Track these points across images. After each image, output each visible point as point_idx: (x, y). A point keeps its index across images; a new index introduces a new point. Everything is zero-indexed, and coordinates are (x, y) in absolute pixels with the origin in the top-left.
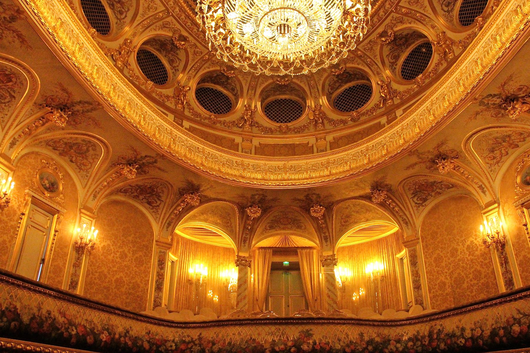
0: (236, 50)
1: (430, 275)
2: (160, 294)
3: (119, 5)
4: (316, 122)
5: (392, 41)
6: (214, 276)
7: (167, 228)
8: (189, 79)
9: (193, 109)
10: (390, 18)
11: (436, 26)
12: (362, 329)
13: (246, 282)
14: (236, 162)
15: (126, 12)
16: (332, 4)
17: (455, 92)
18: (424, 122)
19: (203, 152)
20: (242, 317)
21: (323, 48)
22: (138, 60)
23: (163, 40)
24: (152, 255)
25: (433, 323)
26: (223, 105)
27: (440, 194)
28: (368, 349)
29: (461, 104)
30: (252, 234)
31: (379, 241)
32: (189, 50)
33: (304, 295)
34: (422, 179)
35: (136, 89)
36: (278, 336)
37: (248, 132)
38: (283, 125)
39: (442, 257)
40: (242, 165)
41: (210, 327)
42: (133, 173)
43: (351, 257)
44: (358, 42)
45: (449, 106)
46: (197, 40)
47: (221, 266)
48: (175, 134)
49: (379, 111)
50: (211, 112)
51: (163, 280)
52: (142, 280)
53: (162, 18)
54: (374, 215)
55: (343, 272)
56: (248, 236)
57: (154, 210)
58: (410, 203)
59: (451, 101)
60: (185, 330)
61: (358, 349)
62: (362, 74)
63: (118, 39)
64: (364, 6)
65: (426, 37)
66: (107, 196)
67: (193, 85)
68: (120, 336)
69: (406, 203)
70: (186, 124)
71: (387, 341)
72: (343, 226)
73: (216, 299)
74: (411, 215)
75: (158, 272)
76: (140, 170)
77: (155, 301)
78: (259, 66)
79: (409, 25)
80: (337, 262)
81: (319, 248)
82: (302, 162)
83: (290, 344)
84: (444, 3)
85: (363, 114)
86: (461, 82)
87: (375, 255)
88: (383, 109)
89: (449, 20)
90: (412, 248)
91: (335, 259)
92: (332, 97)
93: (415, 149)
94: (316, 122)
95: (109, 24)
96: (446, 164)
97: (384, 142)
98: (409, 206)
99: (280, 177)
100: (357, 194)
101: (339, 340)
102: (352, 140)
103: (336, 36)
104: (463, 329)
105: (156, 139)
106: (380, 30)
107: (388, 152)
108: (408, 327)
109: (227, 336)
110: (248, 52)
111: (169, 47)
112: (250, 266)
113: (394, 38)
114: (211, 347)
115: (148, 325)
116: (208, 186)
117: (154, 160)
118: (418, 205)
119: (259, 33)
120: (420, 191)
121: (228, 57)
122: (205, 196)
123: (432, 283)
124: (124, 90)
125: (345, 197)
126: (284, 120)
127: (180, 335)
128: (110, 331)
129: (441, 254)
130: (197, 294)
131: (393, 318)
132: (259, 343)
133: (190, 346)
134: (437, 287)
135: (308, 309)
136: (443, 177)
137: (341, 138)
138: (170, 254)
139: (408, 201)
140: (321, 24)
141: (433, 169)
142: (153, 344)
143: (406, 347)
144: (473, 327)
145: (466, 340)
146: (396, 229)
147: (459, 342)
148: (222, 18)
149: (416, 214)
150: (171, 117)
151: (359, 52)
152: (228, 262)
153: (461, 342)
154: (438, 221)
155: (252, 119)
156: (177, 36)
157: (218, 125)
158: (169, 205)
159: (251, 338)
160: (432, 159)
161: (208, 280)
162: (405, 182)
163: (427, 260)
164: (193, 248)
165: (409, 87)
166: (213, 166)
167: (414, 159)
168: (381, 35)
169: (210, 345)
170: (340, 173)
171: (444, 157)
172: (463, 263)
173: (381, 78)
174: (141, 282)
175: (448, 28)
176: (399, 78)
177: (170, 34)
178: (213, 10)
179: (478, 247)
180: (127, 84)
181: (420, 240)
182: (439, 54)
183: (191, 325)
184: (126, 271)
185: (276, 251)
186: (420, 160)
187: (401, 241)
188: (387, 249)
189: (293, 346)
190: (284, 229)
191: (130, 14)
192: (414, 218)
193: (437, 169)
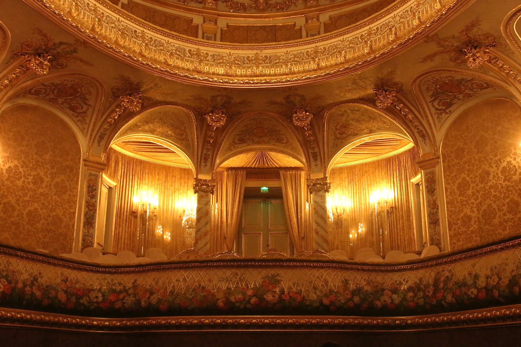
2: (91, 231)
7: (99, 142)
12: (347, 275)
13: (207, 213)
19: (143, 37)
24: (78, 178)
25: (440, 268)
28: (353, 301)
30: (216, 149)
31: (389, 160)
33: (288, 230)
34: (447, 74)
40: (198, 54)
41: (148, 271)
43: (351, 181)
47: (177, 192)
48: (101, 11)
51: (96, 212)
52: (65, 212)
54: (381, 124)
55: (339, 201)
56: (210, 153)
57: (80, 118)
61: (339, 301)
66: (10, 99)
68: (25, 285)
69: (423, 109)
71: (379, 291)
72: (338, 139)
73: (168, 237)
74: (430, 125)
75: (87, 202)
76: (54, 63)
77: (84, 240)
80: (330, 187)
82: (280, 51)
83: (250, 293)
87: (382, 179)
91: (327, 183)
93: (433, 33)
96: (478, 55)
99: (249, 72)
100: (356, 96)
101: (315, 288)
105: (73, 18)
107: (397, 38)
109: (169, 283)
114: (149, 298)
115: (65, 270)
116: (152, 85)
118: (440, 112)
120: (443, 93)
122: (149, 99)
123: (453, 217)
125: (338, 99)
127: (108, 282)
128: (9, 278)
129: (468, 179)
132: (209, 291)
133: (121, 296)
134: (459, 222)
136: (473, 73)
138: (104, 176)
141: (458, 61)
143: (404, 299)
144: (489, 273)
145: (479, 290)
149: (437, 124)
152: (186, 188)
153: (472, 292)
158: (99, 111)
159: (200, 285)
163: (449, 187)
164: (137, 169)
166: (157, 57)
167: (433, 48)
169: (148, 294)
170: (332, 66)
171: (475, 44)
179: (516, 170)
181: (441, 160)
183: (123, 269)
185: (250, 172)
186: (441, 48)
189: (253, 296)
190: (258, 143)
193: (465, 61)
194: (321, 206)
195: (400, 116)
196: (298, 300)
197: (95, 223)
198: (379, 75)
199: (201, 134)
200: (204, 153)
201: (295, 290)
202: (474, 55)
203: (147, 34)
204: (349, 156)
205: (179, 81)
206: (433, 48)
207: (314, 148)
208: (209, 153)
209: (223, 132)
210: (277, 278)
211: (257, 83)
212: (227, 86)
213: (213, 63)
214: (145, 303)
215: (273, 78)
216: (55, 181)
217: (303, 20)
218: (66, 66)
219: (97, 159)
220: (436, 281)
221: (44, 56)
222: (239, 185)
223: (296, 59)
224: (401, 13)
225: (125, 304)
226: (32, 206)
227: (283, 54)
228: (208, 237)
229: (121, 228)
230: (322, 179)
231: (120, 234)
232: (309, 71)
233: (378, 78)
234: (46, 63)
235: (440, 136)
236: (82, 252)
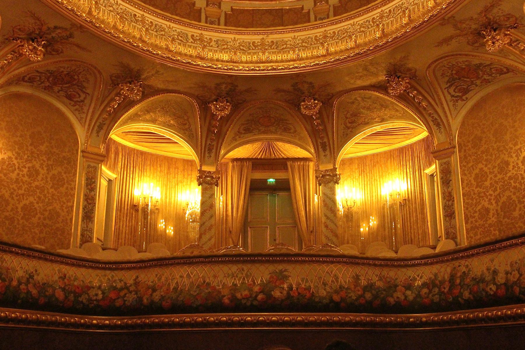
1: (468, 199)
7: (98, 132)
12: (358, 270)
13: (212, 206)
19: (143, 21)
24: (76, 171)
25: (457, 263)
27: (489, 82)
28: (364, 297)
31: (401, 151)
33: (296, 224)
36: (240, 278)
40: (201, 40)
41: (150, 267)
43: (362, 172)
47: (180, 185)
51: (95, 206)
55: (349, 194)
56: (214, 143)
57: (77, 107)
60: (116, 272)
61: (350, 297)
69: (438, 96)
71: (392, 287)
73: (170, 231)
74: (445, 113)
75: (85, 195)
76: (49, 49)
77: (82, 235)
80: (340, 178)
82: (287, 36)
83: (256, 289)
87: (395, 170)
90: (444, 161)
91: (336, 175)
93: (449, 15)
96: (498, 37)
99: (255, 58)
100: (367, 83)
101: (325, 284)
104: (495, 272)
107: (411, 21)
109: (172, 280)
114: (151, 295)
117: (68, 33)
118: (456, 99)
120: (459, 79)
127: (109, 279)
129: (485, 169)
130: (145, 225)
132: (214, 288)
133: (122, 294)
134: (476, 215)
138: (103, 168)
139: (440, 93)
141: (476, 45)
142: (71, 292)
143: (419, 295)
144: (509, 269)
145: (498, 287)
147: (488, 289)
149: (452, 112)
153: (491, 289)
154: (484, 122)
158: (97, 99)
159: (204, 282)
160: (476, 30)
161: (162, 205)
162: (436, 67)
163: (465, 178)
166: (158, 42)
167: (449, 31)
170: (341, 51)
171: (495, 26)
172: (515, 182)
181: (457, 149)
183: (123, 265)
184: (38, 194)
185: (256, 164)
186: (458, 31)
188: (412, 160)
189: (260, 292)
190: (265, 132)
193: (483, 45)
198: (392, 61)
201: (303, 286)
202: (493, 38)
208: (213, 143)
210: (285, 273)
212: (232, 73)
213: (216, 49)
215: (279, 64)
216: (51, 174)
218: (62, 52)
219: (96, 150)
220: (452, 277)
221: (38, 41)
223: (304, 44)
226: (27, 199)
227: (290, 39)
228: (213, 231)
230: (331, 170)
232: (318, 57)
233: (390, 63)
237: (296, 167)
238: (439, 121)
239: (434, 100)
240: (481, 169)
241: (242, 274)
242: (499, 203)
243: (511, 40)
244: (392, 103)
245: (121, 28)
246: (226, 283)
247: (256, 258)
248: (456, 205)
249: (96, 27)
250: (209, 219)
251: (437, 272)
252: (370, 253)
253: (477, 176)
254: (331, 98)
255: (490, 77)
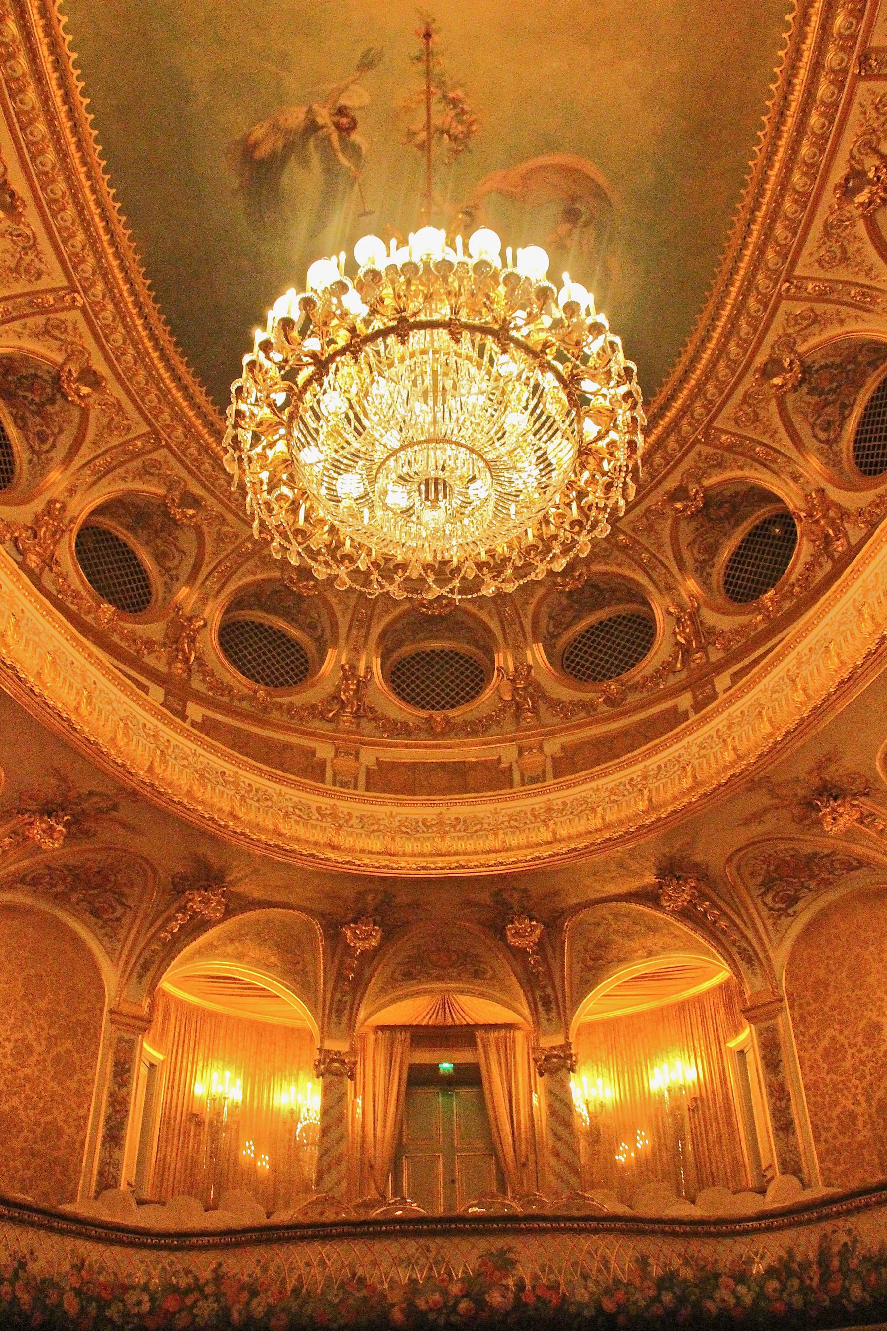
0: (320, 538)
1: (815, 1095)
2: (116, 1153)
3: (38, 420)
4: (519, 707)
5: (699, 510)
6: (260, 1101)
7: (140, 976)
8: (204, 600)
9: (212, 674)
10: (692, 455)
11: (801, 476)
12: (644, 1245)
13: (341, 1119)
14: (319, 809)
15: (56, 436)
16: (550, 433)
17: (852, 635)
18: (780, 706)
19: (236, 785)
20: (330, 1216)
21: (530, 531)
22: (78, 552)
23: (142, 504)
24: (98, 1046)
25: (828, 1226)
26: (287, 664)
27: (831, 884)
28: (661, 1302)
29: (868, 663)
30: (359, 995)
31: (682, 1006)
32: (204, 528)
33: (492, 1150)
34: (782, 846)
35: (69, 625)
37: (348, 732)
38: (438, 716)
39: (842, 1045)
40: (334, 815)
42: (56, 835)
44: (613, 519)
45: (840, 668)
46: (227, 507)
49: (673, 680)
50: (257, 681)
51: (126, 1115)
53: (142, 453)
54: (669, 940)
55: (592, 1089)
57: (108, 929)
58: (757, 910)
59: (844, 657)
60: (179, 1254)
62: (630, 589)
63: (32, 500)
64: (627, 437)
65: (779, 500)
67: (214, 613)
69: (746, 909)
70: (195, 711)
71: (710, 1279)
72: (590, 969)
73: (264, 1164)
74: (760, 938)
75: (111, 1095)
76: (74, 828)
77: (101, 1174)
78: (375, 576)
79: (739, 473)
81: (528, 1026)
83: (455, 1289)
84: (819, 421)
85: (635, 688)
86: (865, 610)
88: (684, 675)
89: (832, 461)
90: (765, 1025)
91: (571, 1056)
92: (558, 647)
94: (519, 707)
95: (12, 463)
96: (841, 810)
97: (686, 757)
98: (756, 916)
99: (428, 847)
101: (585, 1277)
102: (607, 751)
103: (562, 506)
106: (671, 484)
107: (697, 784)
108: (764, 1238)
110: (348, 542)
111: (157, 519)
112: (352, 1077)
113: (704, 504)
114: (248, 1303)
115: (79, 1242)
117: (110, 803)
118: (778, 914)
119: (375, 498)
120: (781, 880)
121: (299, 553)
122: (239, 896)
124: (41, 629)
125: (593, 896)
126: (438, 703)
127: (164, 1269)
129: (841, 1038)
130: (215, 1152)
131: (723, 1213)
132: (373, 1288)
133: (189, 1301)
134: (834, 1125)
135: (505, 1193)
137: (579, 747)
140: (527, 475)
141: (806, 822)
142: (90, 1299)
143: (762, 1295)
146: (723, 974)
148: (285, 461)
149: (773, 938)
150: (157, 693)
151: (622, 537)
155: (359, 700)
156: (176, 495)
157: (275, 715)
158: (146, 915)
159: (354, 1275)
160: (804, 797)
162: (740, 859)
163: (806, 1055)
164: (201, 1032)
165: (744, 619)
166: (260, 820)
167: (763, 799)
168: (673, 496)
170: (579, 835)
171: (835, 792)
173: (677, 599)
174: (66, 1121)
175: (831, 481)
176: (720, 599)
177: (161, 491)
178: (264, 443)
180: (49, 613)
181: (786, 1003)
182: (813, 541)
183: (194, 1240)
186: (777, 800)
187: (737, 1008)
189: (463, 1296)
190: (439, 979)
191: (65, 441)
192: (768, 946)
193: (819, 822)
194: (561, 1101)
195: (704, 923)
196: (552, 1305)
197: (123, 1138)
198: (667, 850)
199: (333, 958)
200: (336, 999)
201: (544, 1281)
202: (834, 811)
203: (243, 779)
204: (608, 1001)
205: (299, 865)
206: (763, 799)
207: (545, 987)
208: (345, 999)
209: (373, 958)
210: (508, 1255)
211: (442, 868)
212: (388, 873)
213: (360, 831)
214: (241, 1315)
215: (471, 857)
216: (53, 1053)
217: (515, 754)
218: (94, 835)
219: (135, 1010)
220: (824, 1254)
221: (57, 816)
222: (398, 1060)
223: (512, 823)
224: (701, 739)
225: (197, 1319)
227: (489, 814)
228: (344, 1165)
229: (169, 1149)
230: (561, 1046)
231: (168, 1158)
232: (539, 845)
233: (664, 855)
234: (60, 827)
235: (779, 957)
236: (96, 1198)
237: (492, 1040)
238: (751, 953)
239: (739, 915)
240: (833, 1038)
241: (428, 1258)
242: (873, 1102)
243: (862, 814)
244: (667, 924)
245: (199, 794)
246: (396, 1278)
247: (509, 1225)
248: (794, 1108)
249: (159, 792)
250: (337, 1143)
251: (791, 1244)
252: (646, 1208)
253: (827, 1053)
254: (560, 917)
255: (831, 876)
